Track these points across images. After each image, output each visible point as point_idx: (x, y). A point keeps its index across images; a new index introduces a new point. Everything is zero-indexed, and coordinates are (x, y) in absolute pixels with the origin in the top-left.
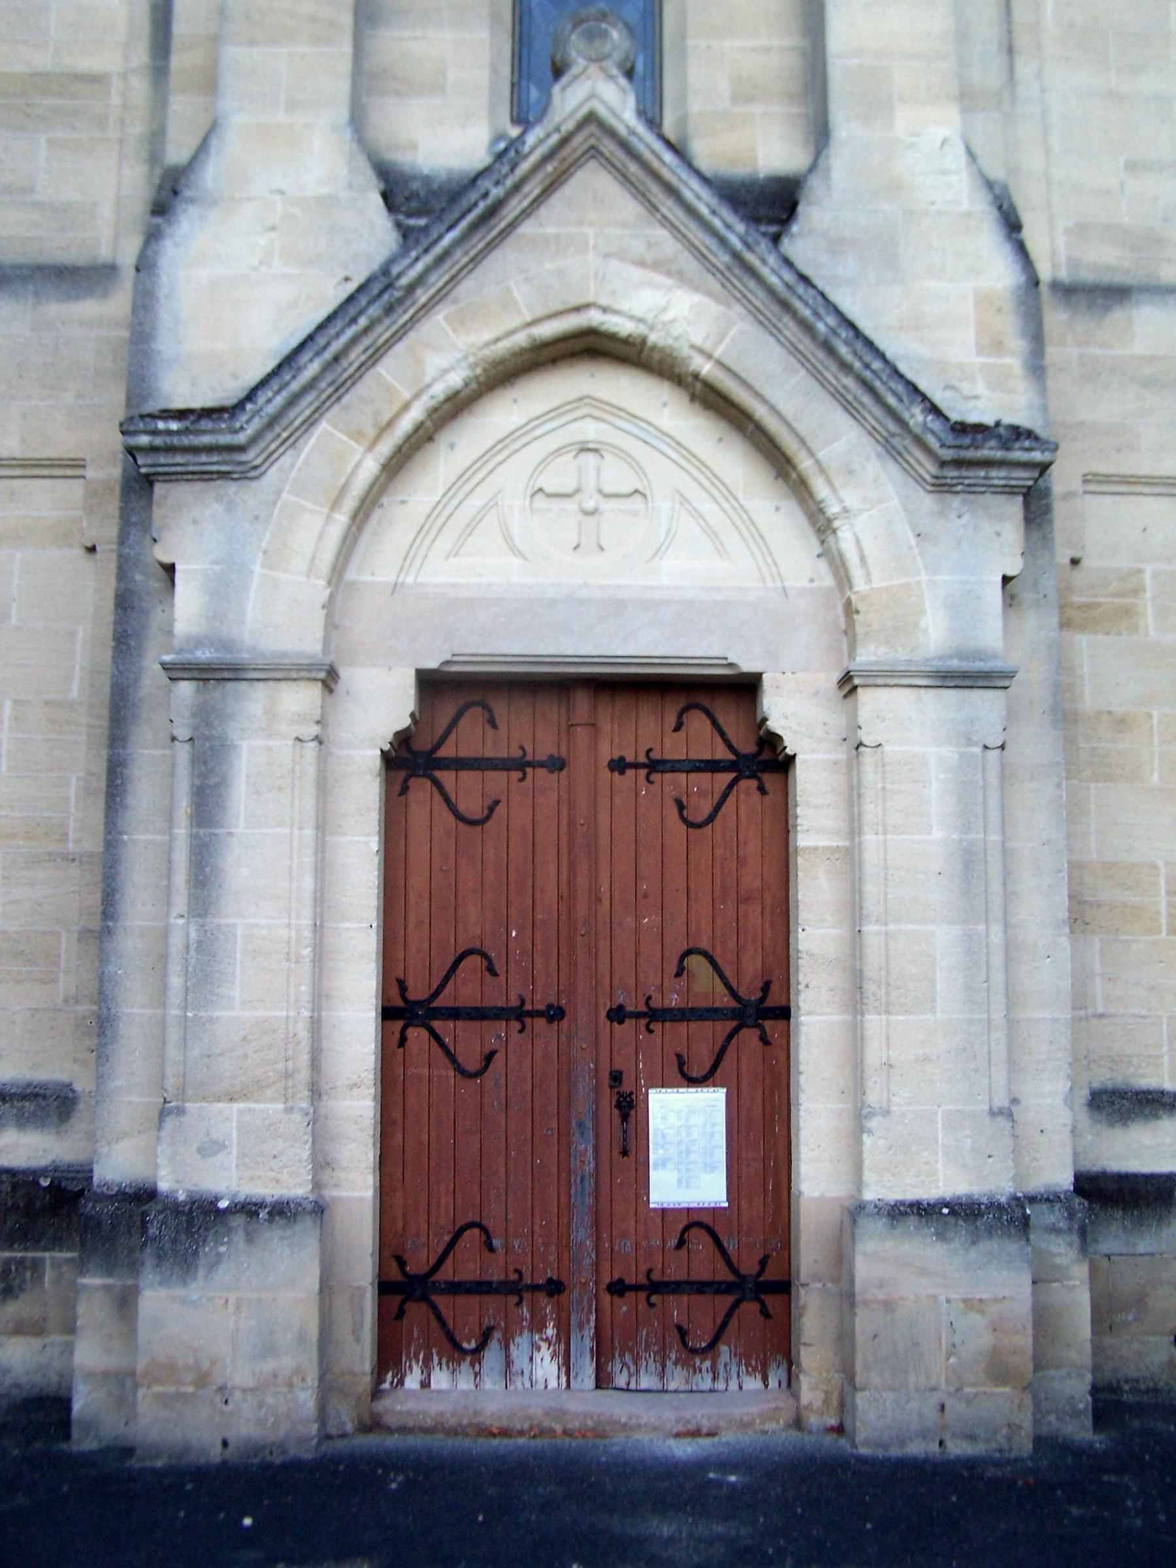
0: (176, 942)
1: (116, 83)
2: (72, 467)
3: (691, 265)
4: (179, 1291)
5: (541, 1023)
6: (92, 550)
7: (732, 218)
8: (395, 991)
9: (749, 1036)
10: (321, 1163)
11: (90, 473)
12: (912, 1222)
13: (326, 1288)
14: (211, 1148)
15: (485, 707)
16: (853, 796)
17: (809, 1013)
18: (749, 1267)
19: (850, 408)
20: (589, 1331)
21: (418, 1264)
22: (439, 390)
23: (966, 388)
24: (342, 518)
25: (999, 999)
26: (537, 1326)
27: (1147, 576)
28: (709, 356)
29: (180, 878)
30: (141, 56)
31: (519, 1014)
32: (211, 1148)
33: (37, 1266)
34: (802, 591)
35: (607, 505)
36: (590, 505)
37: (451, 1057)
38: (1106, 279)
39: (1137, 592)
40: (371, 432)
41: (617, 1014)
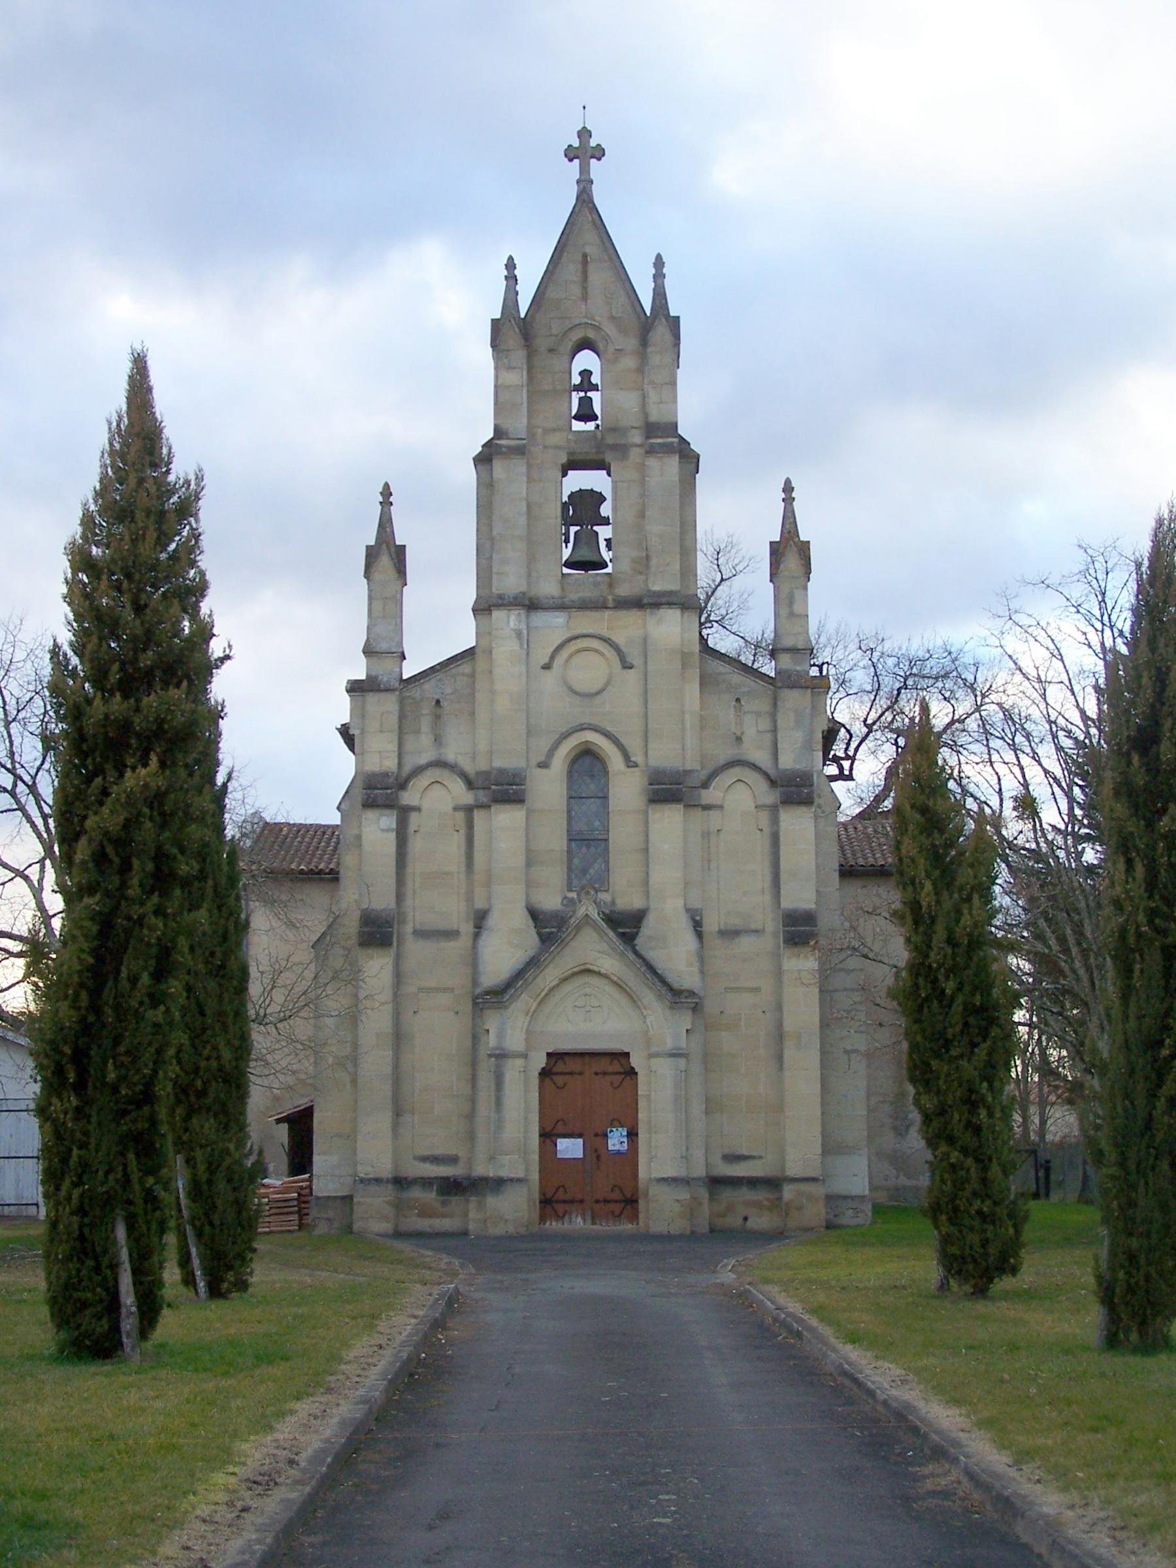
3: (611, 952)
6: (457, 1013)
10: (527, 1170)
11: (456, 992)
18: (629, 1195)
19: (650, 988)
20: (590, 1212)
21: (549, 1196)
24: (528, 1018)
30: (463, 868)
39: (740, 1019)
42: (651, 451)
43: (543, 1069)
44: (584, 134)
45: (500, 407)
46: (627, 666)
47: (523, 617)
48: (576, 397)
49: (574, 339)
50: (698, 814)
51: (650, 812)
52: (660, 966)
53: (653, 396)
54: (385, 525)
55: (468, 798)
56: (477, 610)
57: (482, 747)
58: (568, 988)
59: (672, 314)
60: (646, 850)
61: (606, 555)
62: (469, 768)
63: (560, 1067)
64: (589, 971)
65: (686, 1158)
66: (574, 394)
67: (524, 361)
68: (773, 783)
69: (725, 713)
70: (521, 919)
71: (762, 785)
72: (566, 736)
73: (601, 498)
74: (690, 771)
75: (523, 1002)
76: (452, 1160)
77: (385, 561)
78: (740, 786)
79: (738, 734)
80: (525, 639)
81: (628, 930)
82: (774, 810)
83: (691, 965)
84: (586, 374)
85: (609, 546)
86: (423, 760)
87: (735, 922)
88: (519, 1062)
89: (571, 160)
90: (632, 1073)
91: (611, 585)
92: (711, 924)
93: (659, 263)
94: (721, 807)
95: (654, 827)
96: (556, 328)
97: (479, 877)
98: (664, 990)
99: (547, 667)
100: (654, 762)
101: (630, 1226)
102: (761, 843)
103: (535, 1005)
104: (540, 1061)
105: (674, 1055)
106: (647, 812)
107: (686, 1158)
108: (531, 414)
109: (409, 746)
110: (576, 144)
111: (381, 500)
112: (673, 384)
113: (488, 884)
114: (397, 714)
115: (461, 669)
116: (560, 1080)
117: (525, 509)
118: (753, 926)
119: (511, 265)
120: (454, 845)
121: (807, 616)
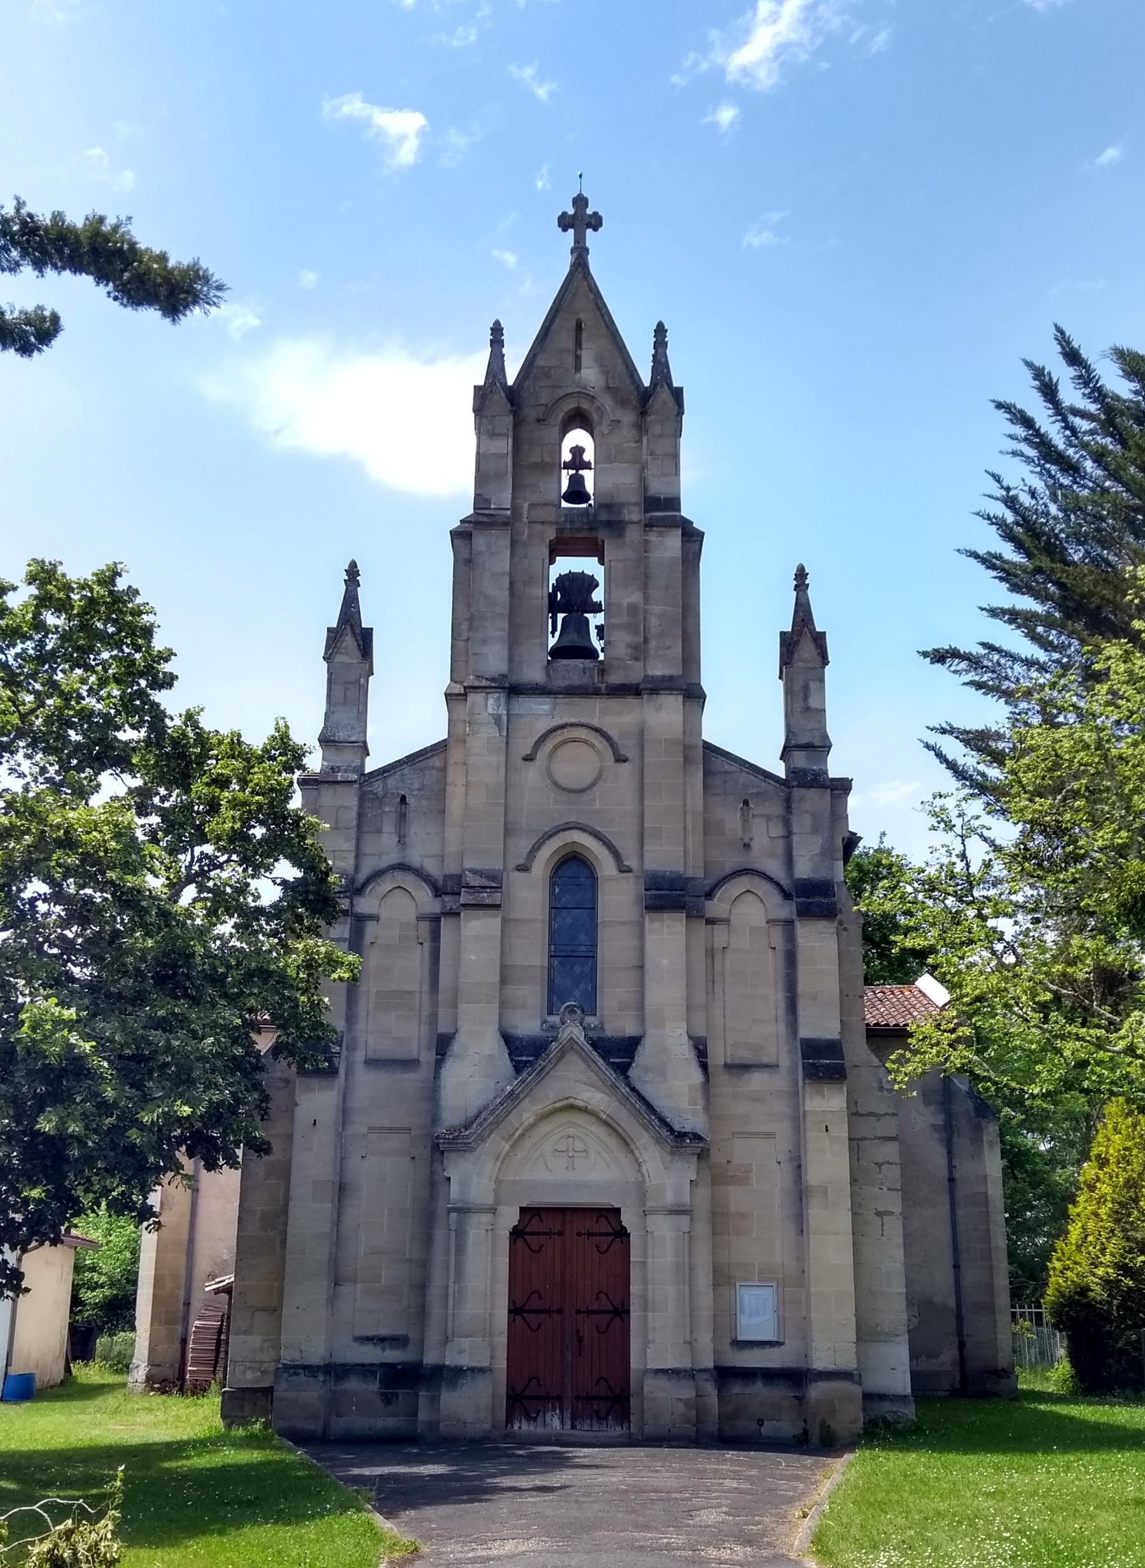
0: (451, 1290)
1: (418, 995)
2: (407, 1130)
3: (599, 1083)
4: (452, 1394)
5: (555, 1314)
7: (612, 1072)
8: (512, 1305)
9: (618, 1319)
12: (660, 1374)
13: (493, 1395)
14: (461, 1352)
15: (540, 1216)
16: (645, 1246)
17: (902, 1293)
22: (526, 1123)
23: (685, 1116)
24: (499, 1163)
25: (687, 1308)
26: (554, 1409)
27: (754, 1167)
28: (605, 1113)
29: (452, 1272)
30: (426, 987)
31: (548, 1311)
32: (461, 1352)
33: (397, 1395)
34: (633, 1182)
35: (575, 1154)
36: (571, 1154)
37: (529, 1325)
38: (744, 1062)
40: (507, 1137)
41: (578, 1312)
42: (649, 525)
43: (515, 1227)
44: (580, 202)
45: (482, 477)
46: (621, 759)
47: (503, 700)
48: (565, 476)
49: (566, 410)
50: (700, 925)
51: (647, 923)
52: (658, 1103)
53: (652, 472)
54: (350, 604)
55: (433, 906)
56: (450, 695)
57: (452, 847)
58: (545, 1127)
59: (675, 384)
60: (641, 967)
61: (597, 644)
62: (432, 868)
63: (535, 1226)
64: (572, 1107)
65: (691, 1344)
66: (564, 472)
67: (511, 428)
68: (787, 896)
69: (731, 819)
70: (491, 1045)
71: (774, 897)
72: (548, 836)
73: (592, 583)
74: (692, 878)
75: (496, 1143)
76: (398, 1341)
77: (349, 641)
78: (750, 897)
79: (747, 840)
80: (507, 726)
81: (619, 1060)
82: (789, 924)
83: (695, 1103)
84: (577, 451)
85: (601, 635)
86: (385, 862)
87: (743, 1055)
88: (486, 1218)
89: (565, 229)
90: (623, 1234)
91: (602, 673)
92: (717, 1056)
93: (660, 331)
94: (726, 921)
95: (651, 939)
96: (545, 398)
97: (442, 996)
98: (665, 1133)
99: (529, 758)
100: (651, 866)
101: (618, 1429)
102: (772, 965)
103: (507, 1147)
104: (510, 1218)
105: (677, 1211)
106: (641, 925)
107: (690, 1343)
108: (516, 487)
109: (369, 847)
110: (571, 211)
111: (347, 578)
112: (675, 456)
113: (454, 1005)
114: (356, 808)
115: (431, 762)
116: (534, 1241)
117: (507, 585)
118: (765, 1060)
119: (497, 331)
120: (416, 961)
121: (824, 710)
